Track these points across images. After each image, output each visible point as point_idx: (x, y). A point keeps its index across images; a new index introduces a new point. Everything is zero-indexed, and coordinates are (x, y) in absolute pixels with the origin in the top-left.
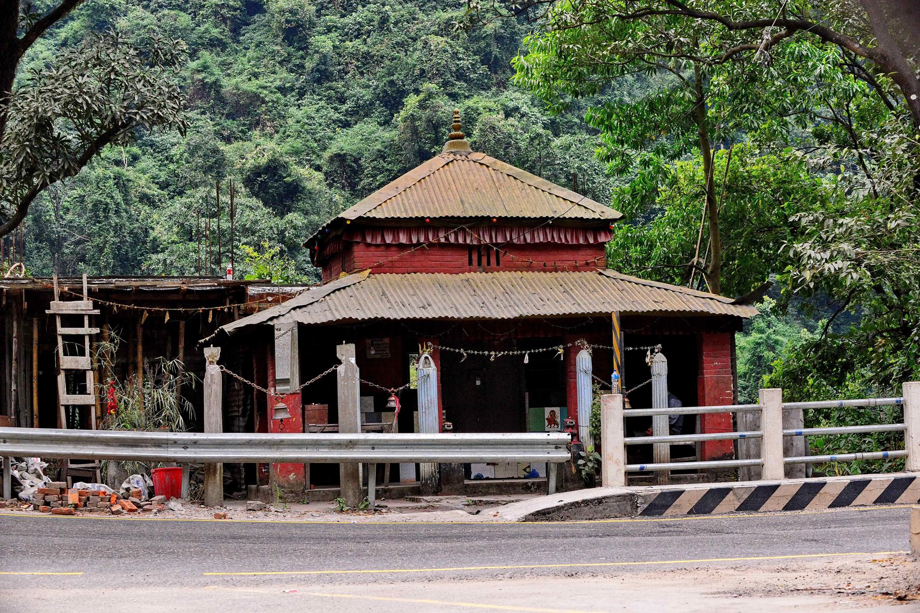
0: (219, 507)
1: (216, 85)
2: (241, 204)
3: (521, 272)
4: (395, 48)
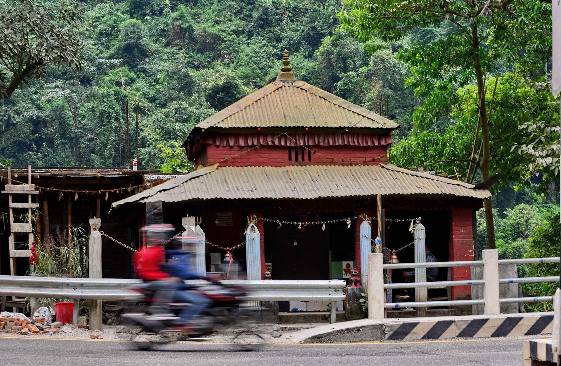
0: (97, 330)
1: (190, 29)
3: (326, 165)
4: (316, 3)
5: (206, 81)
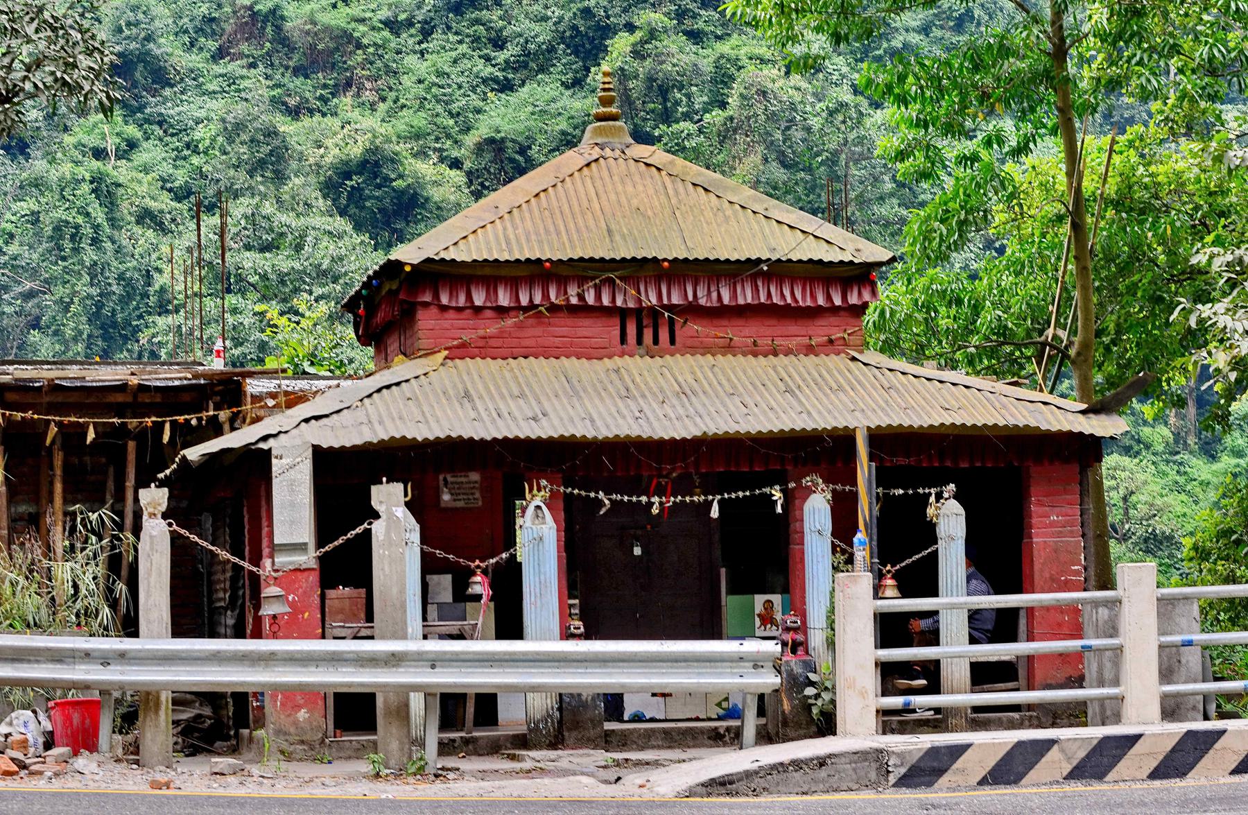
0: (163, 768)
2: (314, 228)
5: (320, 147)
